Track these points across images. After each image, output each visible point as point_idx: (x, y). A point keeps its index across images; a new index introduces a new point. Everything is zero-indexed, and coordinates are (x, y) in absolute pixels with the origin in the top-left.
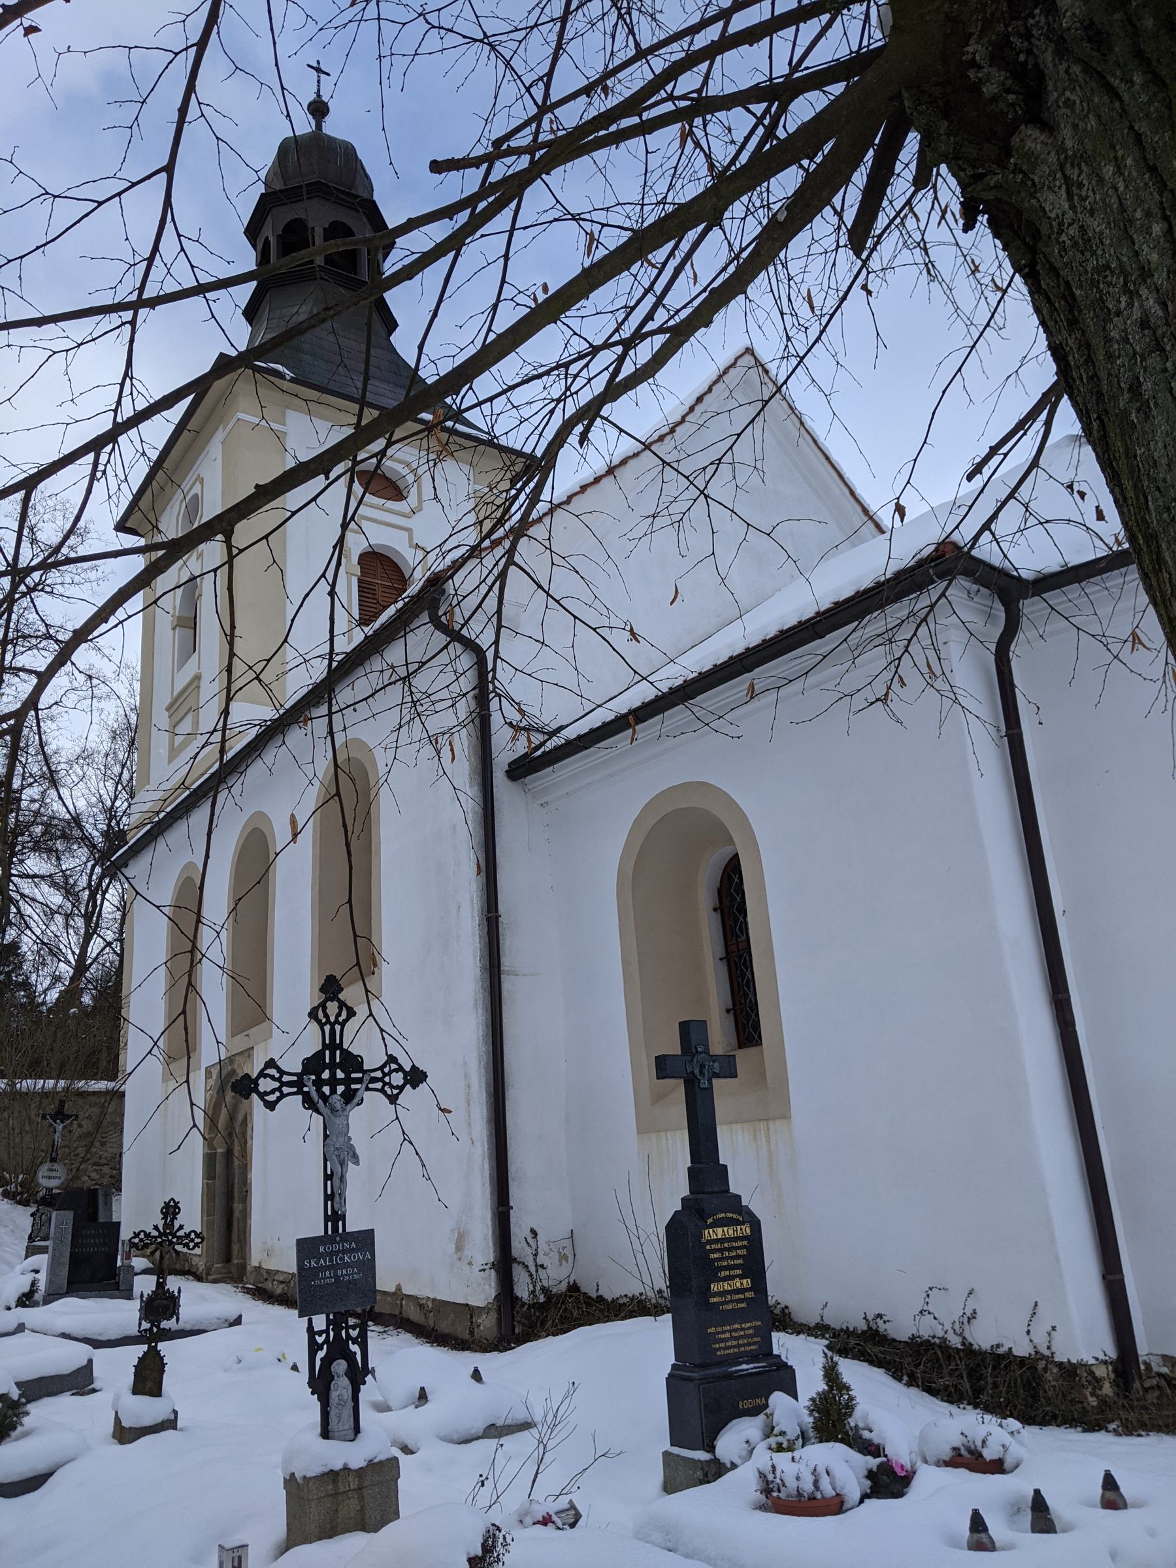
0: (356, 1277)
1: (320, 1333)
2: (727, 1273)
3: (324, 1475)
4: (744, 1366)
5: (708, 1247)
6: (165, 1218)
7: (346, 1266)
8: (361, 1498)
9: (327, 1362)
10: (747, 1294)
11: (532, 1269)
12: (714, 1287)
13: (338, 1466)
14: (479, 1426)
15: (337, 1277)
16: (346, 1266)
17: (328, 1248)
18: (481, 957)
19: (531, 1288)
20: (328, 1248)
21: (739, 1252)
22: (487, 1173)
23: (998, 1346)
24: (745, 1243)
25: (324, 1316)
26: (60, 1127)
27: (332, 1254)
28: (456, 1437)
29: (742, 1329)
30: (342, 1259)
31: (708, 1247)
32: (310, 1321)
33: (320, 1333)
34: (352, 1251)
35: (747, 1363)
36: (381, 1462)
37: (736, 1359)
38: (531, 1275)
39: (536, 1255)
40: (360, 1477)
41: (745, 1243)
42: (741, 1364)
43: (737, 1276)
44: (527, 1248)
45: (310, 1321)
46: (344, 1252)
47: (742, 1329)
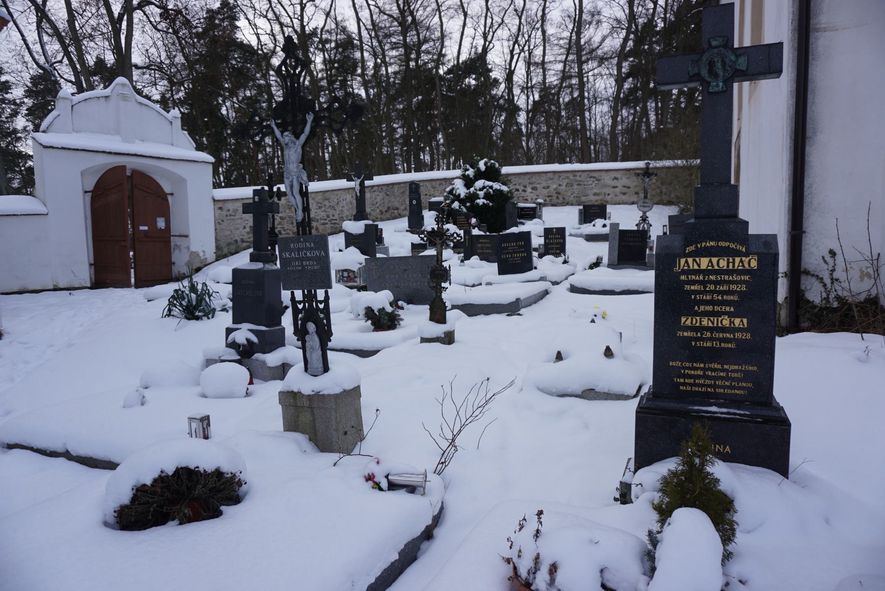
0: (316, 267)
1: (300, 302)
2: (709, 308)
3: (288, 392)
4: (714, 409)
5: (683, 277)
6: (438, 224)
7: (309, 259)
8: (313, 414)
9: (305, 321)
10: (738, 335)
11: (828, 281)
12: (686, 321)
13: (296, 390)
14: (578, 388)
15: (303, 266)
16: (309, 259)
17: (297, 245)
18: (793, 20)
19: (824, 295)
20: (297, 245)
21: (733, 287)
22: (787, 204)
23: (738, 524)
24: (747, 278)
25: (301, 291)
26: (647, 180)
27: (299, 250)
28: (554, 391)
29: (723, 370)
30: (305, 254)
31: (683, 277)
32: (293, 294)
33: (300, 302)
34: (311, 249)
35: (719, 406)
36: (324, 395)
37: (707, 398)
38: (825, 285)
39: (833, 270)
40: (310, 400)
41: (747, 278)
42: (711, 405)
43: (725, 313)
44: (826, 267)
45: (293, 294)
46: (307, 249)
47: (726, 371)
